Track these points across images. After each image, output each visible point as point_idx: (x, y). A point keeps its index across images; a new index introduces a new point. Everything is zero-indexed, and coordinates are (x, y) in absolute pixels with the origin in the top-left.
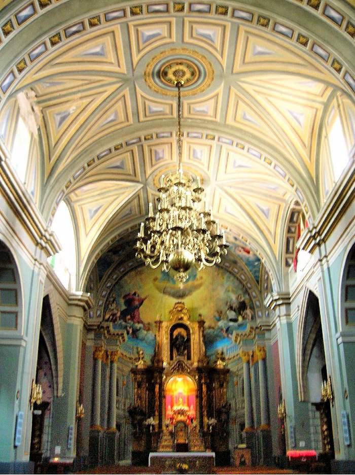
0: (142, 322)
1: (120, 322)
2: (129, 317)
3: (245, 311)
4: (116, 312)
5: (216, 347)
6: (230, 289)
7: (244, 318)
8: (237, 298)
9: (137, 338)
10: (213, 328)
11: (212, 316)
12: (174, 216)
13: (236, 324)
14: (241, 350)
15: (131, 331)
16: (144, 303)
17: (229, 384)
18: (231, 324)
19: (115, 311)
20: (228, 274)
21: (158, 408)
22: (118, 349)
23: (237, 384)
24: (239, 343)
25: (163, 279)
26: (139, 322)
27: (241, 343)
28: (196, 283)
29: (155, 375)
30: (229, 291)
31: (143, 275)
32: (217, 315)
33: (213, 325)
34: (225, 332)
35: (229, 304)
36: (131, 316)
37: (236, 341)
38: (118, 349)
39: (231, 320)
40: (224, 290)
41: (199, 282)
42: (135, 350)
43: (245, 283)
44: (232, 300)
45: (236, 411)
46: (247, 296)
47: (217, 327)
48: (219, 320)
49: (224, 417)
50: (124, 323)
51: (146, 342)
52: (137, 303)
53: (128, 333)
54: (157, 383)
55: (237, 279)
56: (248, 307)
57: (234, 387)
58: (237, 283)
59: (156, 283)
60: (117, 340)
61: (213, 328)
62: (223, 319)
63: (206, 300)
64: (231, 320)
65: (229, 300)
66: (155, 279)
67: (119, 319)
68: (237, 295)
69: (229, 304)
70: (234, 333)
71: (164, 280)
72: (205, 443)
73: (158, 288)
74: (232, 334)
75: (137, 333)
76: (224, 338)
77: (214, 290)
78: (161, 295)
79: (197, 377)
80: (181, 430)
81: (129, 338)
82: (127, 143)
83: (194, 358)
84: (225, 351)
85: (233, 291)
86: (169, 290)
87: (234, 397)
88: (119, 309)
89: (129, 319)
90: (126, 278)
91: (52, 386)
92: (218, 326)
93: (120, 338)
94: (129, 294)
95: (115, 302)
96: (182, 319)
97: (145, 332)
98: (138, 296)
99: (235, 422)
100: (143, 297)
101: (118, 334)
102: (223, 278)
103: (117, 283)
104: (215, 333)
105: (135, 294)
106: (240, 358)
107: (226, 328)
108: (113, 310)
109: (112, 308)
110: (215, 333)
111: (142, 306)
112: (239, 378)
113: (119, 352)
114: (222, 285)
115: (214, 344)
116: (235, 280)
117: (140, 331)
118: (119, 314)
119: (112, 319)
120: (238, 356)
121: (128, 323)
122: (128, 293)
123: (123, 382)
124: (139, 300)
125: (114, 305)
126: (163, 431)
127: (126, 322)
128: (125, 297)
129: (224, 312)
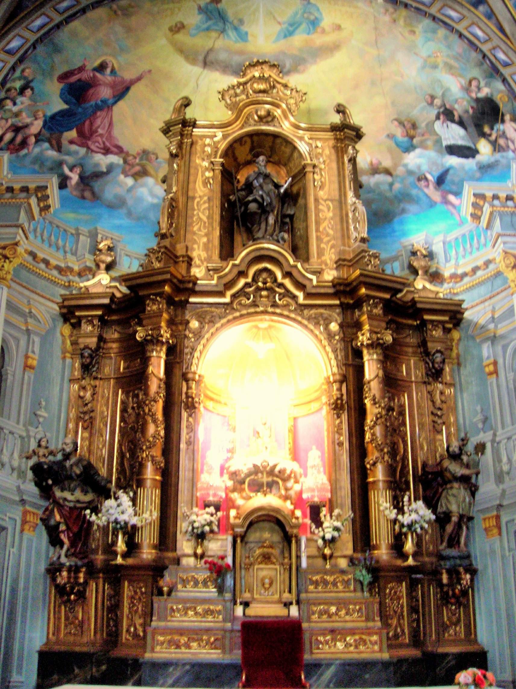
0: (120, 150)
1: (37, 150)
2: (73, 134)
3: (500, 127)
4: (28, 120)
5: (404, 234)
6: (440, 61)
7: (495, 145)
8: (467, 89)
9: (95, 197)
10: (388, 172)
11: (383, 137)
12: (292, 132)
13: (469, 163)
14: (499, 246)
15: (74, 177)
16: (131, 93)
17: (463, 371)
18: (454, 161)
19: (26, 119)
20: (427, 22)
21: (157, 452)
22: (20, 237)
23: (496, 372)
24: (489, 226)
25: (205, 26)
26: (107, 151)
27: (497, 223)
28: (318, 40)
29: (151, 307)
30: (435, 67)
31: (133, 18)
32: (399, 132)
33: (387, 163)
34: (431, 186)
35: (438, 102)
36: (81, 133)
37: (476, 217)
38: (20, 237)
39: (453, 150)
40: (419, 63)
41: (329, 39)
42: (85, 241)
43: (485, 48)
44: (446, 91)
45: (500, 478)
46: (499, 86)
47: (400, 170)
48: (409, 148)
49: (465, 442)
50: (52, 154)
51: (129, 214)
52: (105, 93)
53: (63, 185)
54: (156, 341)
55: (461, 35)
56: (507, 117)
57: (483, 383)
58: (459, 46)
59: (180, 37)
60: (20, 206)
61: (388, 172)
62: (424, 147)
63: (356, 87)
64: (453, 150)
65: (439, 93)
66: (179, 28)
67: (37, 141)
68: (464, 82)
69: (438, 102)
70: (468, 191)
71: (208, 29)
72: (384, 616)
73: (181, 50)
74: (458, 194)
75: (97, 185)
76: (432, 204)
77: (381, 62)
78: (197, 70)
79: (334, 327)
80: (266, 558)
81: (64, 201)
82: (211, 57)
83: (320, 253)
84: (437, 248)
85: (450, 68)
86: (223, 56)
87: (485, 420)
88: (40, 114)
89: (71, 142)
90: (75, 24)
91: (157, 587)
92: (405, 166)
93: (33, 201)
94: (81, 69)
95: (28, 92)
96: (269, 118)
97: (130, 181)
98: (113, 71)
99: (499, 528)
100: (128, 75)
101: (25, 189)
102: (413, 32)
103: (40, 40)
104: (397, 186)
105: (102, 68)
106: (498, 274)
107: (437, 174)
108: (17, 115)
109: (15, 109)
110: (397, 186)
111: (121, 103)
112: (499, 349)
113: (20, 250)
114: (411, 49)
115: (396, 225)
116: (454, 38)
117: (110, 177)
118: (37, 126)
119: (13, 140)
120: (491, 267)
121: (68, 153)
122: (79, 64)
123: (27, 357)
124: (113, 86)
125: (23, 101)
126: (177, 561)
127: (59, 149)
128: (63, 77)
129: (422, 125)
